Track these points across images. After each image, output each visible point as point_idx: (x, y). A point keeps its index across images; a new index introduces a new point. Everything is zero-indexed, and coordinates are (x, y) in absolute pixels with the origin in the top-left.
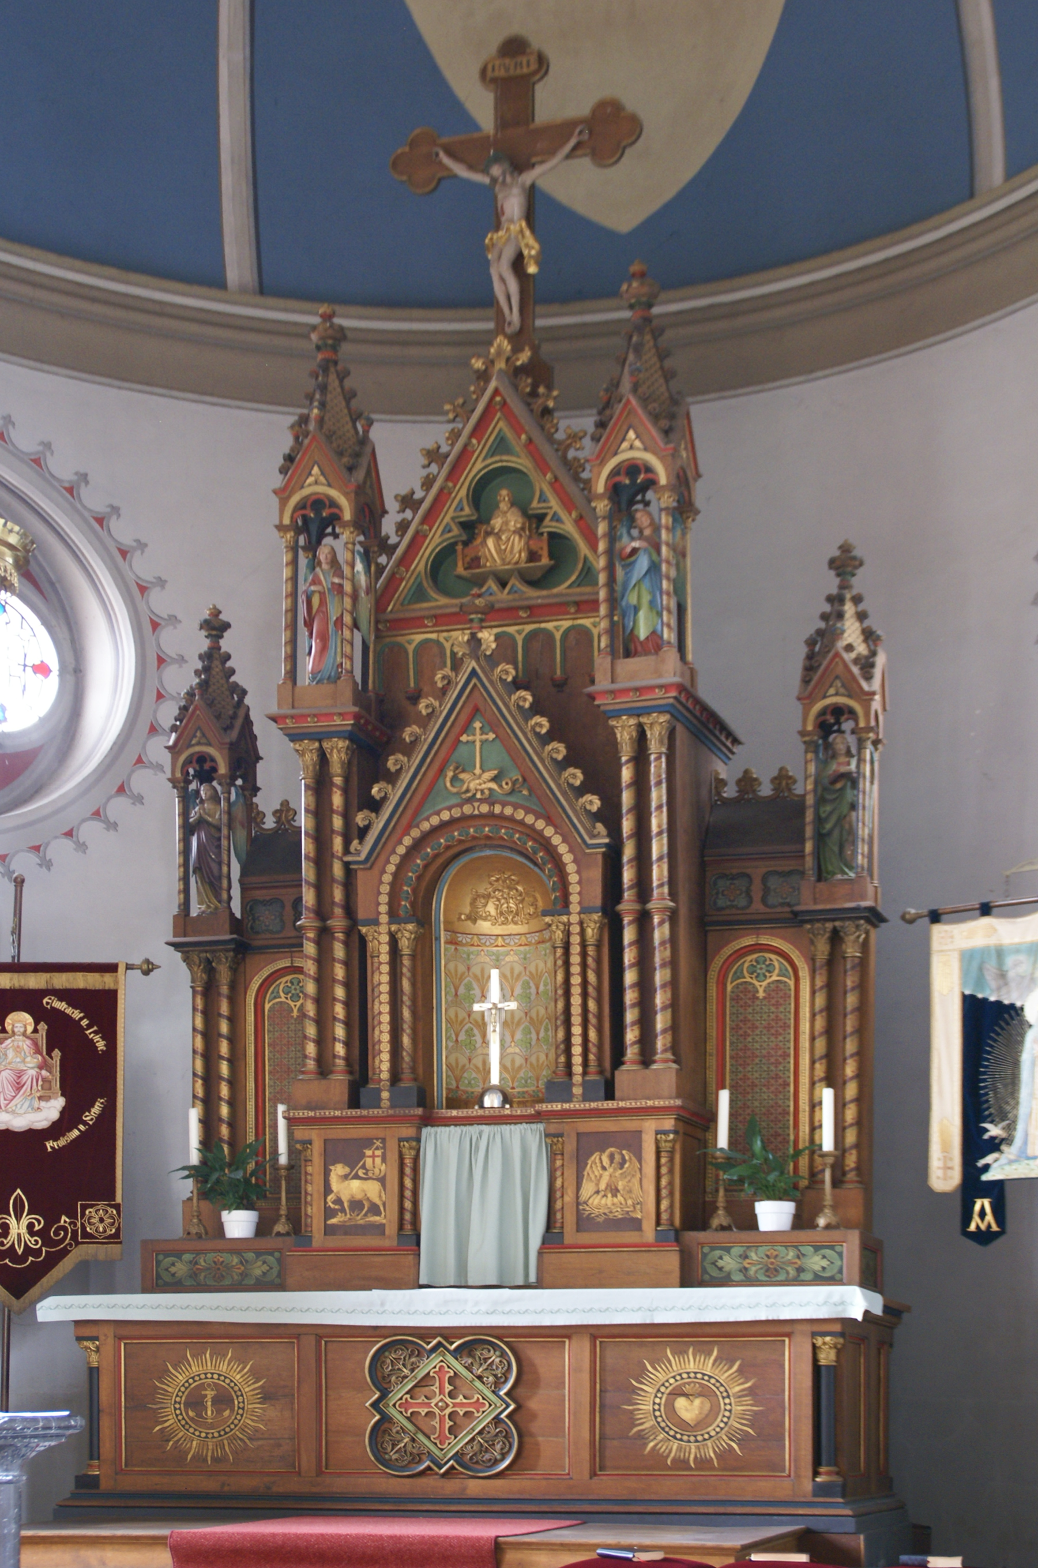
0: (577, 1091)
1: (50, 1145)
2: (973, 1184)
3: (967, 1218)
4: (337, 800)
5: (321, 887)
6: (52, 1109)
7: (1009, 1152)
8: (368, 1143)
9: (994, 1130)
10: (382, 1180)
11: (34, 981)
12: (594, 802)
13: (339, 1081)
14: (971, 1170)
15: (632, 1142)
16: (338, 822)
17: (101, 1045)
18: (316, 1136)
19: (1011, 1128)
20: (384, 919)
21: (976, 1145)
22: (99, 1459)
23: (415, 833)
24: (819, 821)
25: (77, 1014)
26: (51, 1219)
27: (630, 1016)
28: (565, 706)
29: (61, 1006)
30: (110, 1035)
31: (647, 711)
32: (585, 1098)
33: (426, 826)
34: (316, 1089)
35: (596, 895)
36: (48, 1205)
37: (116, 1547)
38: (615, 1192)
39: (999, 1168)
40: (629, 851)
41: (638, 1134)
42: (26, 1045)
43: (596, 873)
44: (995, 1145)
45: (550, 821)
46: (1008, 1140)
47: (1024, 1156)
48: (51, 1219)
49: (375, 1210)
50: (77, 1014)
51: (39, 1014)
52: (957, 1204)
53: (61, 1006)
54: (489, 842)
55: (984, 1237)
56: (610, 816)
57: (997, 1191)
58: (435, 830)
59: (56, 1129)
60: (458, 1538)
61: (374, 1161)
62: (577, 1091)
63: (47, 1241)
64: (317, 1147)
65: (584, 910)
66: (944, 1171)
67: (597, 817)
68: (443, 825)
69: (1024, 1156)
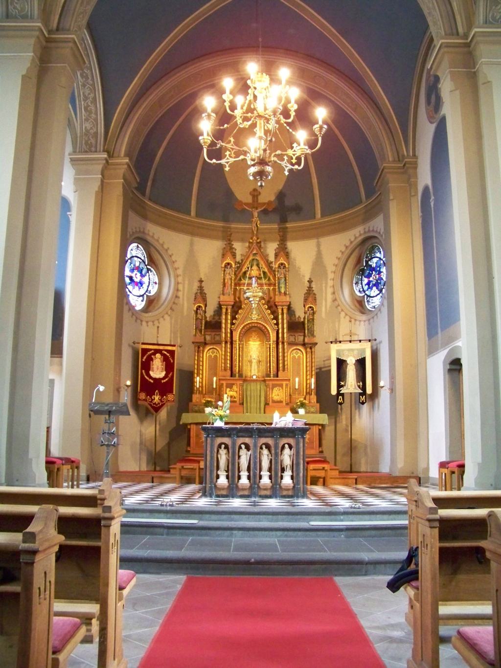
0: (272, 376)
1: (162, 381)
2: (339, 394)
3: (338, 400)
4: (229, 317)
5: (226, 333)
6: (163, 374)
7: (345, 388)
8: (234, 384)
9: (342, 383)
10: (236, 392)
11: (161, 348)
12: (275, 322)
13: (229, 372)
14: (338, 391)
15: (281, 386)
16: (229, 322)
17: (172, 361)
18: (224, 383)
19: (345, 383)
20: (238, 340)
21: (339, 386)
22: (250, 413)
23: (243, 325)
24: (308, 326)
25: (168, 355)
26: (162, 396)
27: (281, 362)
28: (272, 307)
29: (165, 353)
30: (173, 359)
31: (284, 306)
32: (274, 377)
33: (245, 324)
34: (224, 373)
35: (275, 339)
36: (163, 394)
37: (31, 549)
38: (278, 395)
39: (343, 390)
40: (280, 331)
41: (282, 384)
42: (159, 360)
43: (275, 334)
44: (342, 386)
45: (267, 323)
46: (345, 385)
47: (347, 388)
48: (162, 396)
49: (235, 398)
50: (168, 355)
51: (162, 354)
52: (336, 398)
53: (165, 353)
54: (255, 327)
55: (341, 404)
56: (277, 324)
57: (343, 395)
58: (247, 324)
59: (164, 378)
60: (457, 276)
61: (235, 388)
62: (272, 376)
63: (162, 402)
64: (225, 385)
65: (273, 341)
66: (334, 391)
67: (275, 324)
68: (249, 324)
69: (347, 388)
